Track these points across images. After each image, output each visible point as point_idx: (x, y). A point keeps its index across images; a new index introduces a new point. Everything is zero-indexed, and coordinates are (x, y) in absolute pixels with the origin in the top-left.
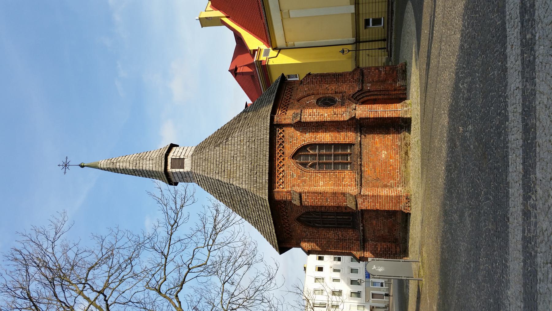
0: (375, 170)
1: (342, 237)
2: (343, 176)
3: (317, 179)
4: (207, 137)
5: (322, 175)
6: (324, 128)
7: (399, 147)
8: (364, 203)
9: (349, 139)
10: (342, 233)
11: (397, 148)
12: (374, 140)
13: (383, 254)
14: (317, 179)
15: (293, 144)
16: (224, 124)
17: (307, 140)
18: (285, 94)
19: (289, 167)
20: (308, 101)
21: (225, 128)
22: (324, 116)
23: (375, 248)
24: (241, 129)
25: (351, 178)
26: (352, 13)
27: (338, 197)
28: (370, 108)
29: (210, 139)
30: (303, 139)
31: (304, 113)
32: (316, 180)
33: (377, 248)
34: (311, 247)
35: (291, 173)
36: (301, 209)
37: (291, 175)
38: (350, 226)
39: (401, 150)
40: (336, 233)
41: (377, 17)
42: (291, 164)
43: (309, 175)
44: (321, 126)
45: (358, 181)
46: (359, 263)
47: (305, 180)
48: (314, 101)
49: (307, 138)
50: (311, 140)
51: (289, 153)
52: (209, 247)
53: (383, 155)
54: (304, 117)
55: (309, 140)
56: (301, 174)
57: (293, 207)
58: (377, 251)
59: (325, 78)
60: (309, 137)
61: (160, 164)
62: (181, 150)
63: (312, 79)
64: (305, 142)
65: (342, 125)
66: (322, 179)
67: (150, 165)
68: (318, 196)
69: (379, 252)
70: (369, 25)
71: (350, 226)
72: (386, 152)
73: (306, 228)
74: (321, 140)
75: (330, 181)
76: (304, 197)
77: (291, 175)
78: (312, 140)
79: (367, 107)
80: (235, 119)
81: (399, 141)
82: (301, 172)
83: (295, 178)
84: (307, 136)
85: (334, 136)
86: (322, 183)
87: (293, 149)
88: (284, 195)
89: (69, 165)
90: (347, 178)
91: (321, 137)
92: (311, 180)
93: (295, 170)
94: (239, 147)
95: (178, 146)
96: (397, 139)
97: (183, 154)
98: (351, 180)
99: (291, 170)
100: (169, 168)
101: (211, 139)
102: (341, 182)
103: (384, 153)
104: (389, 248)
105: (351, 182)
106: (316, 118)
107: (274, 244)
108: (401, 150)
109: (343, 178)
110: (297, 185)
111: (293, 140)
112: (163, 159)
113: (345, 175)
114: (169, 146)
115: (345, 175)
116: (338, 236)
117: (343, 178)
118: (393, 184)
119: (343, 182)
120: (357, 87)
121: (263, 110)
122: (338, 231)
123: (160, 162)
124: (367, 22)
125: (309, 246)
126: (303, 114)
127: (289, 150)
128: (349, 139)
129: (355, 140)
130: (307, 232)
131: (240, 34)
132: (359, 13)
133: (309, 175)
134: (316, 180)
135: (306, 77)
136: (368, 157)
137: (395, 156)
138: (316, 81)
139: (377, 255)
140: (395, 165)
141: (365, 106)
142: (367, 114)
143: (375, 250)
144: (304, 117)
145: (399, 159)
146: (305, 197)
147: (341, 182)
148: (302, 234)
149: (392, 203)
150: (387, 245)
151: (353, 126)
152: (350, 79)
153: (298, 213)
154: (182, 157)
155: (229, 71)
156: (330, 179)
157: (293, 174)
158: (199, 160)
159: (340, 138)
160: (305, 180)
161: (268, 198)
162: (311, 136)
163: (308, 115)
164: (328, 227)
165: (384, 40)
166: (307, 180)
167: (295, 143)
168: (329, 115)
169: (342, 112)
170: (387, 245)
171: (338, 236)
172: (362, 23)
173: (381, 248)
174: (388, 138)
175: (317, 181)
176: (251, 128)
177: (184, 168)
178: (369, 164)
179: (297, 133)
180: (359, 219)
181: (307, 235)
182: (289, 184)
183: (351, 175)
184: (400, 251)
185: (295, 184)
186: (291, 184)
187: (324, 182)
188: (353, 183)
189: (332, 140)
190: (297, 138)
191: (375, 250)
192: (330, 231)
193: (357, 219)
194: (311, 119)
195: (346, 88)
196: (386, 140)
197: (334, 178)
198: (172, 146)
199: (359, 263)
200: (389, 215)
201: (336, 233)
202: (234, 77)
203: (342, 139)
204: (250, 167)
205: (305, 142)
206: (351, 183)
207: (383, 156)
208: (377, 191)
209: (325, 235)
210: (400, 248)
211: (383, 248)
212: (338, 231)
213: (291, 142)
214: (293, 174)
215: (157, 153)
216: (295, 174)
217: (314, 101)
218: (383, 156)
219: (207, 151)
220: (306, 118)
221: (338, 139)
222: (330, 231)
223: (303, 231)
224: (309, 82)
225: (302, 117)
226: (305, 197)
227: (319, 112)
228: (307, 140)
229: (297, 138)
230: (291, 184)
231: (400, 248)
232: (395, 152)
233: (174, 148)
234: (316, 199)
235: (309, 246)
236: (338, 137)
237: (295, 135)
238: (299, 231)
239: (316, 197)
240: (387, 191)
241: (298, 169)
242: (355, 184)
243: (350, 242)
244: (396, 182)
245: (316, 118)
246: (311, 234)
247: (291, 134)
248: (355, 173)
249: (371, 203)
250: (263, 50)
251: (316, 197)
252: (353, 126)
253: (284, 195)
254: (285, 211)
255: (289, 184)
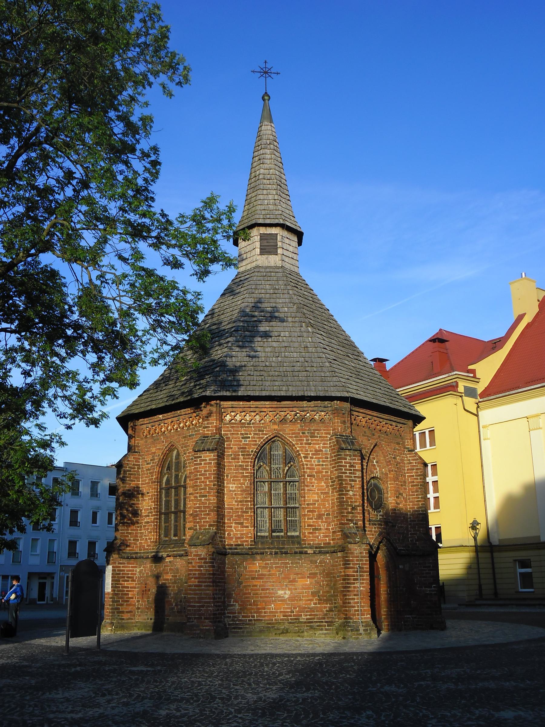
0: (257, 579)
1: (146, 522)
2: (246, 523)
3: (240, 480)
4: (315, 292)
5: (247, 487)
6: (329, 490)
7: (296, 619)
8: (199, 559)
9: (309, 533)
10: (151, 522)
11: (294, 615)
12: (308, 577)
13: (118, 591)
14: (240, 480)
15: (301, 437)
16: (337, 320)
17: (308, 461)
18: (388, 422)
19: (259, 431)
20: (377, 462)
21: (330, 321)
22: (349, 491)
23: (128, 577)
24: (327, 347)
25: (243, 538)
26: (539, 536)
27: (208, 514)
28: (363, 568)
29: (311, 295)
30: (309, 454)
31: (354, 456)
32: (237, 477)
33: (128, 581)
34: (128, 471)
35: (250, 434)
36: (189, 453)
37: (247, 434)
38: (162, 536)
39: (291, 623)
40: (151, 513)
41: (534, 580)
42: (266, 434)
43: (247, 466)
44: (331, 486)
45: (236, 549)
46: (104, 551)
47: (238, 459)
48: (377, 472)
49: (310, 461)
50: (307, 468)
51: (285, 430)
52: (118, 298)
53: (283, 592)
54: (347, 455)
55: (307, 465)
56: (248, 451)
57: (192, 438)
58: (123, 581)
59: (417, 491)
60: (312, 465)
61: (268, 216)
62: (291, 249)
63: (417, 469)
64: (305, 457)
65: (334, 521)
66: (240, 487)
67: (266, 201)
68: (209, 482)
69: (121, 584)
70: (523, 567)
71: (162, 536)
72: (287, 596)
73: (159, 461)
74: (307, 486)
75: (236, 501)
76: (207, 456)
77: (247, 434)
78: (308, 470)
79: (365, 564)
80: (347, 339)
81: (307, 619)
82: (252, 451)
83: (241, 441)
84: (314, 462)
85: (315, 508)
86: (232, 487)
87: (291, 437)
88: (211, 423)
89: (270, 76)
90: (243, 530)
91: (313, 486)
92: (238, 469)
93: (256, 441)
94: (296, 345)
95: (300, 243)
96: (310, 615)
97: (286, 253)
98: (239, 538)
99: (255, 434)
100: (263, 230)
101: (310, 299)
102: (234, 520)
103: (285, 593)
104: (128, 601)
105: (236, 538)
106: (346, 476)
107: (134, 407)
108: (291, 623)
109: (242, 524)
110: (230, 445)
111: (307, 436)
112: (276, 221)
113: (247, 527)
114: (299, 229)
115: (247, 527)
116: (146, 516)
117: (242, 524)
118: (232, 608)
119: (235, 523)
120: (403, 547)
121: (219, 356)
122: (154, 515)
123: (272, 216)
124: (524, 564)
125: (129, 467)
126: (352, 453)
127: (291, 430)
128: (309, 533)
129: (309, 544)
130: (153, 463)
131: (501, 347)
132: (539, 549)
133: (247, 466)
134: (237, 477)
135: (420, 458)
136: (278, 567)
137: (281, 612)
138: (413, 476)
139: (116, 581)
140: (265, 613)
141: (366, 560)
142: (353, 564)
143: (124, 577)
144: (347, 455)
145: (276, 620)
146: (207, 459)
147: (234, 520)
148: (149, 454)
149: (199, 606)
150: (132, 598)
151: (333, 540)
152: (416, 534)
153: (182, 448)
154: (280, 251)
155: (440, 330)
156: (241, 501)
157: (249, 437)
158: (275, 278)
159: (312, 519)
160: (238, 459)
161: (206, 396)
162: (314, 469)
163: (350, 463)
164: (161, 498)
165: (496, 594)
166: (238, 462)
167: (302, 440)
168: (351, 498)
169: (356, 520)
170: (132, 598)
171: (146, 516)
172: (522, 555)
173: (128, 587)
174: (312, 600)
175: (236, 480)
176: (327, 364)
177: (261, 254)
178: (267, 567)
179: (318, 444)
180: (174, 551)
181: (148, 464)
182: (230, 431)
183: (248, 537)
184: (123, 619)
185: (231, 441)
186: (231, 434)
187: (235, 491)
188: (234, 542)
189: (308, 504)
190: (310, 444)
191: (124, 577)
192: (154, 502)
193: (173, 548)
194: (212, 457)
195: (401, 527)
196: (308, 596)
197: (242, 509)
198: (299, 235)
199: (104, 551)
200: (181, 601)
201: (151, 513)
202: (431, 338)
203: (310, 522)
204: (261, 364)
205: (305, 457)
206: (232, 538)
207: (280, 592)
208: (219, 582)
209: (148, 493)
210: (128, 619)
211: (127, 591)
212: (154, 515)
213: (303, 433)
214: (249, 437)
215: (287, 211)
216: (249, 441)
217: (377, 472)
218: (280, 592)
219: (291, 292)
220: (346, 459)
221: (310, 515)
222: (154, 502)
223: (153, 457)
224: (410, 463)
225: (347, 452)
226: (207, 459)
227: (356, 481)
228: (308, 461)
229: (310, 444)
230: (231, 434)
231: (128, 619)
232: (288, 612)
233: (296, 239)
234: (204, 478)
235: (129, 467)
236: (313, 515)
237: (316, 440)
238: (153, 450)
239: (208, 478)
240: (219, 598)
241: (256, 447)
242: (232, 545)
243: (137, 536)
244: (235, 613)
245: (346, 476)
246: (149, 470)
247: (318, 433)
248: (251, 545)
249: (199, 570)
250: (475, 387)
251: (208, 478)
252: (333, 540)
253: (211, 423)
254: (186, 426)
255: (230, 431)
